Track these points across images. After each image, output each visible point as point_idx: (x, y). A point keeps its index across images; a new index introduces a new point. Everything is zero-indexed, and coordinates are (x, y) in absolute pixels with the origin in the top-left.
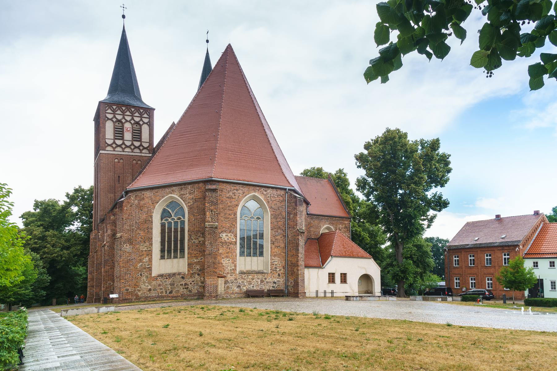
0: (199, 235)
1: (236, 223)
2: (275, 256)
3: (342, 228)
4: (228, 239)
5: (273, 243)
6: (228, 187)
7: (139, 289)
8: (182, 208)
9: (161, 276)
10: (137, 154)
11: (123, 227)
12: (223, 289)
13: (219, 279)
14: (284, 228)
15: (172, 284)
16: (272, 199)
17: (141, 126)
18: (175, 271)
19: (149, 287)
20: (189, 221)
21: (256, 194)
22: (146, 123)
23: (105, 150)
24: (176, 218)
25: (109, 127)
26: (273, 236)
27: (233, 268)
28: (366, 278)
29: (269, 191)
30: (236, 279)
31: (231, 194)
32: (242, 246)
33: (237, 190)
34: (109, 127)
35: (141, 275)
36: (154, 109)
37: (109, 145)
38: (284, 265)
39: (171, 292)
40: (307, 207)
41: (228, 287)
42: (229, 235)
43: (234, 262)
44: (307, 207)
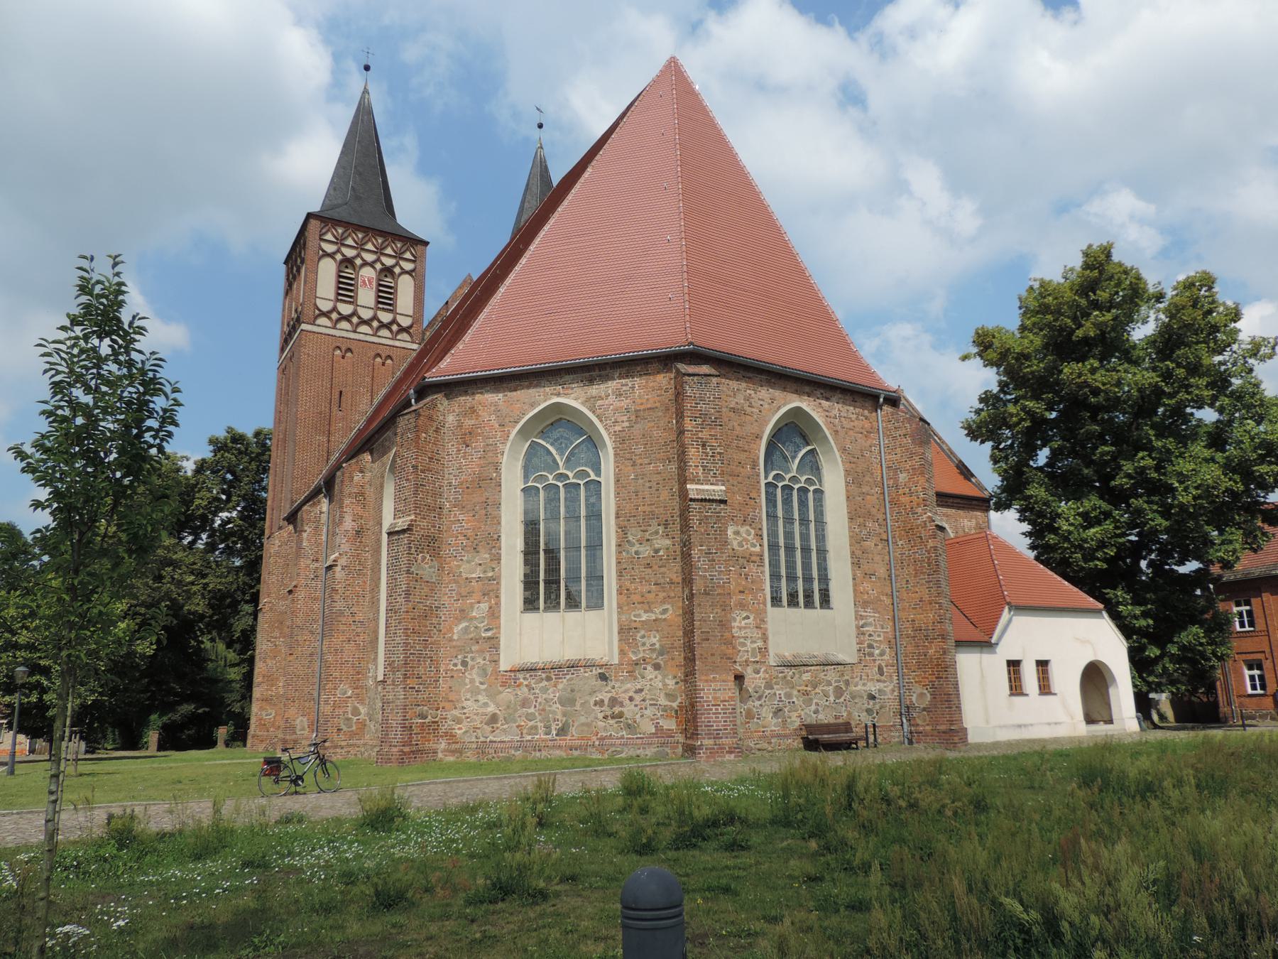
0: (652, 529)
2: (865, 604)
4: (740, 545)
7: (456, 713)
14: (881, 517)
15: (568, 701)
18: (570, 654)
19: (491, 709)
21: (804, 406)
24: (570, 475)
26: (856, 540)
27: (760, 644)
28: (1095, 677)
30: (769, 686)
31: (740, 399)
34: (327, 271)
35: (464, 663)
38: (891, 636)
39: (562, 731)
42: (743, 530)
43: (760, 625)
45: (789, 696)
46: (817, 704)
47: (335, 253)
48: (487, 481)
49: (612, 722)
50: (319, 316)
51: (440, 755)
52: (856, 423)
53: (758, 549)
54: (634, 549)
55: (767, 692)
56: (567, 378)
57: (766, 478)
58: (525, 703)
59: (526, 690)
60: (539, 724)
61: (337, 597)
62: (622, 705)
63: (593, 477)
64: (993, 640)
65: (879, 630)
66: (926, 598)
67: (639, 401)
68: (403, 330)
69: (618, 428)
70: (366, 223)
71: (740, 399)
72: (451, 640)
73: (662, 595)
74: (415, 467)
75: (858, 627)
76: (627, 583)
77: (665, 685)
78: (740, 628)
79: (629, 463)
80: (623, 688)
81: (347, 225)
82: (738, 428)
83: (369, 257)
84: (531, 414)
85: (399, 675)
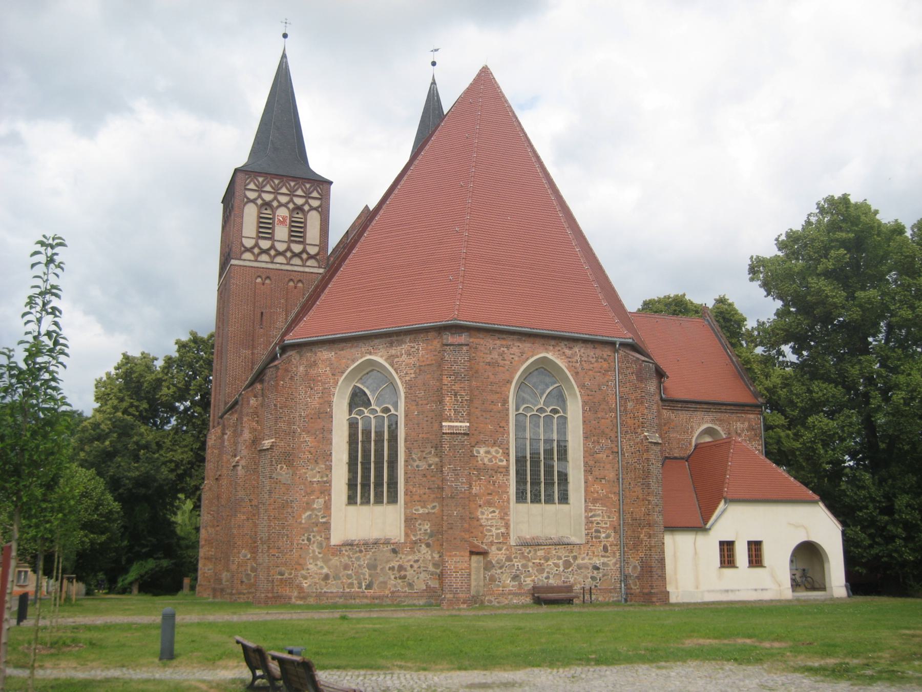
0: (427, 450)
1: (507, 421)
2: (595, 501)
3: (743, 430)
4: (490, 460)
5: (589, 470)
6: (489, 342)
7: (304, 572)
8: (393, 385)
9: (350, 544)
10: (296, 268)
11: (276, 423)
12: (482, 583)
13: (474, 558)
14: (613, 435)
16: (585, 366)
17: (305, 214)
19: (325, 570)
20: (406, 416)
21: (550, 356)
22: (316, 209)
23: (240, 259)
24: (378, 409)
25: (250, 214)
26: (589, 454)
27: (503, 530)
28: (808, 554)
29: (576, 349)
30: (509, 559)
31: (495, 355)
32: (521, 480)
33: (508, 348)
34: (250, 214)
35: (309, 540)
36: (331, 183)
37: (248, 250)
38: (616, 524)
39: (369, 586)
40: (660, 383)
41: (492, 579)
42: (493, 450)
44: (660, 383)
45: (524, 566)
46: (548, 572)
47: (256, 199)
48: (325, 415)
49: (399, 581)
50: (245, 251)
51: (293, 600)
52: (595, 365)
53: (505, 463)
54: (415, 464)
55: (507, 563)
56: (377, 341)
57: (517, 409)
58: (346, 567)
59: (346, 558)
60: (355, 582)
61: (239, 489)
62: (405, 570)
63: (393, 412)
64: (708, 526)
65: (604, 517)
66: (641, 496)
67: (421, 359)
68: (311, 257)
69: (408, 378)
70: (281, 172)
71: (495, 355)
72: (301, 523)
73: (433, 496)
74: (275, 405)
75: (587, 518)
76: (411, 487)
77: (433, 557)
78: (487, 519)
79: (414, 403)
80: (406, 559)
81: (266, 175)
82: (492, 377)
83: (283, 199)
84: (352, 367)
85: (265, 546)
